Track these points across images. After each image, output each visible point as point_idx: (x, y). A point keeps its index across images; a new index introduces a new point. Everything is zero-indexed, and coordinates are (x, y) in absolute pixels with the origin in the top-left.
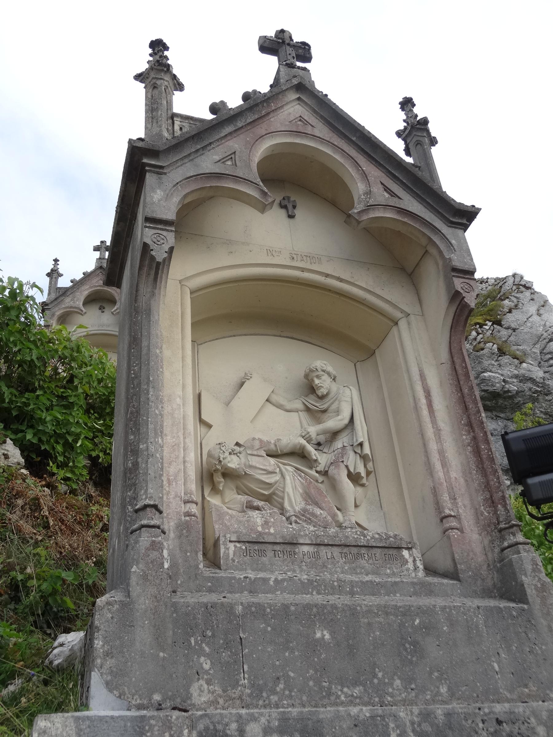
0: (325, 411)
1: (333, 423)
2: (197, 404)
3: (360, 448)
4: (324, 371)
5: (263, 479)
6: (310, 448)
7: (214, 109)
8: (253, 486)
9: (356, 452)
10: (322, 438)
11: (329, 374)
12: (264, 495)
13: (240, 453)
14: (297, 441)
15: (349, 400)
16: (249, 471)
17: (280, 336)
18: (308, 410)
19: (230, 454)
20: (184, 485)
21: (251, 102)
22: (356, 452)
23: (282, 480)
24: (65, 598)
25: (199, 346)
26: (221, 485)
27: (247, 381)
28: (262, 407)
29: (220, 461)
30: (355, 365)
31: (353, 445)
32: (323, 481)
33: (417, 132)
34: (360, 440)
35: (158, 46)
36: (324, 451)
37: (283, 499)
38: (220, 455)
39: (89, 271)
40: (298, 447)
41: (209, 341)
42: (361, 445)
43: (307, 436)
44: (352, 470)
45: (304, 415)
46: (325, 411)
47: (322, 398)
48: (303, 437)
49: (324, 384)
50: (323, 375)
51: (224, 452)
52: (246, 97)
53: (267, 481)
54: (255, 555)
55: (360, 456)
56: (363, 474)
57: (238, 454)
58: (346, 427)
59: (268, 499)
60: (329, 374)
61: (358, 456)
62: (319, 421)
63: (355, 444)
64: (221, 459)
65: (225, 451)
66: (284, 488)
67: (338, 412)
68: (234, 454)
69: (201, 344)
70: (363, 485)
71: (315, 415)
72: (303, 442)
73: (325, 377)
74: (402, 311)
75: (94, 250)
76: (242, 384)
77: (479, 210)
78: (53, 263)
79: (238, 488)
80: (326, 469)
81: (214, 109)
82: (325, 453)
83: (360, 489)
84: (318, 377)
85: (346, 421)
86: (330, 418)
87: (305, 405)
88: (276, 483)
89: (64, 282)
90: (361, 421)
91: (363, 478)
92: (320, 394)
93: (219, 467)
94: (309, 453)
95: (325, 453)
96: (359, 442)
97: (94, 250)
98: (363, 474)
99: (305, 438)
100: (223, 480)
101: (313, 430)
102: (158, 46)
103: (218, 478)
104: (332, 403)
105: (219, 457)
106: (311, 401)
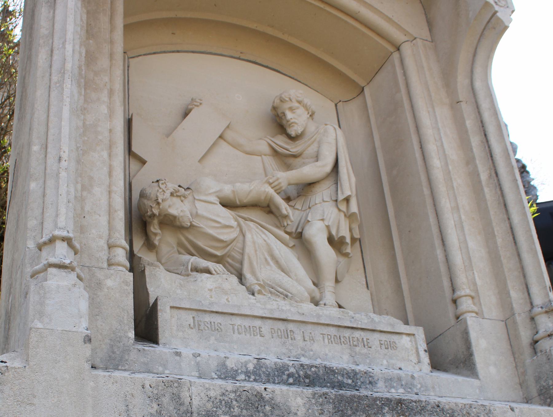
1: (308, 171)
2: (127, 133)
3: (345, 203)
4: (299, 102)
5: (215, 235)
6: (279, 200)
8: (201, 243)
10: (292, 192)
11: (306, 107)
13: (185, 197)
14: (263, 189)
15: (334, 142)
16: (196, 222)
17: (239, 59)
18: (275, 153)
19: (172, 194)
22: (340, 210)
23: (241, 238)
25: (130, 60)
26: (158, 238)
27: (196, 108)
28: (215, 144)
29: (158, 204)
30: (336, 105)
31: (336, 201)
32: (294, 246)
34: (348, 193)
36: (296, 207)
37: (241, 263)
38: (158, 194)
40: (263, 198)
41: (144, 55)
42: (347, 200)
43: (276, 183)
44: (334, 232)
45: (270, 161)
46: (295, 156)
47: (293, 139)
48: (270, 184)
49: (297, 120)
50: (298, 108)
51: (163, 191)
53: (222, 237)
54: (206, 328)
55: (345, 215)
56: (348, 240)
57: (183, 198)
58: (328, 176)
60: (306, 107)
61: (342, 215)
62: (288, 167)
64: (160, 201)
65: (165, 189)
66: (243, 249)
67: (317, 158)
68: (177, 196)
69: (133, 57)
70: (346, 255)
71: (285, 160)
72: (271, 191)
73: (301, 111)
74: (406, 33)
76: (186, 114)
79: (180, 245)
80: (299, 230)
82: (298, 209)
83: (343, 260)
84: (291, 109)
85: (328, 168)
86: (304, 164)
88: (233, 241)
90: (347, 170)
91: (347, 244)
92: (293, 134)
93: (156, 212)
94: (278, 208)
95: (298, 209)
96: (345, 196)
98: (348, 240)
99: (273, 185)
100: (159, 231)
101: (285, 177)
103: (154, 228)
104: (309, 146)
105: (157, 197)
106: (280, 141)
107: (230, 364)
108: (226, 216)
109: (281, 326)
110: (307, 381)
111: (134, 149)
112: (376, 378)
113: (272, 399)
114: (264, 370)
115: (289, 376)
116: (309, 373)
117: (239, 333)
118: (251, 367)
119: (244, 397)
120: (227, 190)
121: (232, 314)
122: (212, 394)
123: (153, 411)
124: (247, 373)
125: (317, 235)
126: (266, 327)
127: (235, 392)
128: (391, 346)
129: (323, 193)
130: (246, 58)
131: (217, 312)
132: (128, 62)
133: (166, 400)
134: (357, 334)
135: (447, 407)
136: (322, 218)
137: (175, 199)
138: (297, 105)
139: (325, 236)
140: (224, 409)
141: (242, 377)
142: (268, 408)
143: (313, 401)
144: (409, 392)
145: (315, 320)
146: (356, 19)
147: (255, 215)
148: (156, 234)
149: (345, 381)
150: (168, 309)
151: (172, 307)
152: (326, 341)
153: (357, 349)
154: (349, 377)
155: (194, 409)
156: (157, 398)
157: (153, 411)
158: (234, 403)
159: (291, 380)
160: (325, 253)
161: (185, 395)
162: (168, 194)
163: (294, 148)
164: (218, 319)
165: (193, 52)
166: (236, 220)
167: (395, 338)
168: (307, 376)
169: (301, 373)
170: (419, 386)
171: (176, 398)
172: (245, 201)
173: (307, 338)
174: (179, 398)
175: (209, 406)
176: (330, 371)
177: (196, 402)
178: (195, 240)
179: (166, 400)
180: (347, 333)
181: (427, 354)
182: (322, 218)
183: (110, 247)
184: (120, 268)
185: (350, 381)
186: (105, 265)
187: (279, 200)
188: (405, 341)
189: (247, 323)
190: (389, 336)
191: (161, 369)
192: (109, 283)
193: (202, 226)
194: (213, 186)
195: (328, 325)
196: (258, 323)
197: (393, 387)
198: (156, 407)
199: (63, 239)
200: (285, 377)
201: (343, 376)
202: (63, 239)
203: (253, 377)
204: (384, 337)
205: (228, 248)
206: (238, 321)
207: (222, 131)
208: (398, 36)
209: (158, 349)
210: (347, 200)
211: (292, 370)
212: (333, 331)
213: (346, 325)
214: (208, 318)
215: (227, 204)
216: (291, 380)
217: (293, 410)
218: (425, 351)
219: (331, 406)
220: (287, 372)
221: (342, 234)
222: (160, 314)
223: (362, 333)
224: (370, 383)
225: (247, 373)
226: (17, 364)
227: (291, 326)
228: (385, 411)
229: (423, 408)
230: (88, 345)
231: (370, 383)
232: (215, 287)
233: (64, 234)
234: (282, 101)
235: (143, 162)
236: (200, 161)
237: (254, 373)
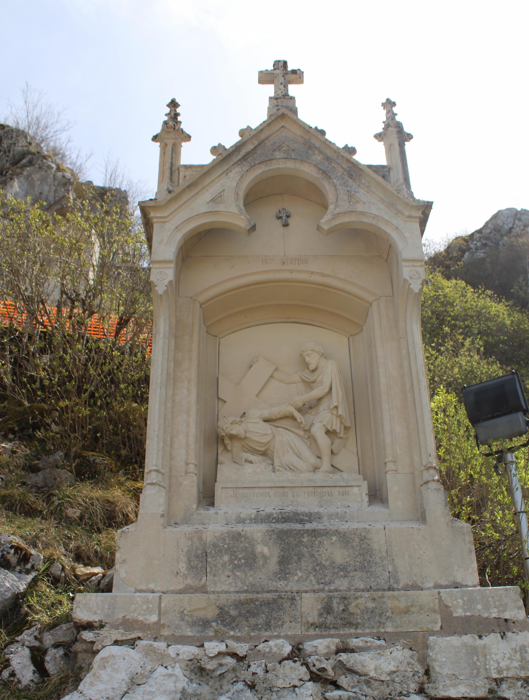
0: (314, 382)
4: (312, 350)
6: (297, 414)
7: (214, 150)
8: (252, 445)
9: (333, 414)
12: (261, 451)
16: (248, 435)
17: (287, 322)
20: (377, 589)
21: (247, 136)
24: (71, 332)
26: (229, 446)
28: (267, 382)
29: (224, 430)
30: (349, 339)
33: (395, 135)
35: (173, 104)
37: (273, 452)
39: (253, 127)
46: (314, 382)
52: (242, 133)
59: (264, 454)
63: (332, 407)
64: (224, 429)
75: (262, 81)
76: (251, 367)
77: (432, 203)
78: (168, 110)
79: (243, 446)
81: (214, 150)
84: (308, 355)
85: (327, 390)
87: (301, 377)
89: (195, 154)
97: (262, 81)
102: (173, 104)
103: (227, 441)
107: (242, 516)
108: (267, 428)
109: (281, 490)
110: (283, 520)
111: (219, 396)
112: (323, 515)
113: (245, 535)
114: (260, 517)
115: (273, 519)
116: (284, 516)
117: (258, 497)
118: (253, 516)
119: (231, 535)
120: (266, 414)
121: (254, 487)
122: (216, 535)
123: (189, 545)
124: (251, 520)
125: (318, 431)
126: (272, 492)
127: (227, 533)
128: (344, 494)
129: (324, 405)
130: (290, 321)
131: (246, 488)
132: (219, 341)
133: (195, 539)
134: (325, 490)
135: (342, 531)
136: (322, 420)
137: (234, 426)
138: (311, 352)
139: (323, 431)
140: (221, 541)
141: (248, 521)
142: (243, 539)
143: (266, 534)
144: (342, 521)
145: (300, 485)
146: (345, 292)
147: (286, 423)
148: (228, 444)
149: (305, 518)
150: (220, 489)
151: (222, 488)
152: (306, 495)
153: (324, 498)
154: (307, 516)
155: (208, 542)
156: (191, 539)
157: (189, 545)
158: (227, 538)
159: (274, 521)
160: (323, 440)
161: (204, 537)
162: (229, 424)
163: (312, 378)
164: (246, 491)
165: (258, 325)
166: (271, 429)
167: (348, 489)
168: (283, 518)
169: (280, 516)
170: (349, 517)
171: (200, 538)
172: (278, 417)
173: (295, 495)
174: (201, 538)
175: (215, 540)
176: (296, 514)
177: (208, 539)
178: (249, 444)
179: (195, 539)
180: (319, 490)
181: (368, 496)
182: (322, 420)
183: (187, 464)
184: (191, 474)
185: (307, 518)
186: (183, 474)
187: (297, 414)
188: (356, 490)
189: (262, 491)
190: (345, 488)
191: (208, 521)
192: (185, 483)
193: (251, 436)
194: (256, 414)
195: (308, 487)
196: (268, 490)
197: (333, 519)
198: (190, 542)
199: (155, 471)
200: (271, 519)
201: (303, 516)
202: (155, 471)
203: (254, 521)
204: (342, 489)
205: (267, 446)
206: (257, 491)
207: (271, 373)
208: (369, 298)
209: (212, 511)
210: (336, 407)
211: (275, 515)
212: (311, 490)
213: (318, 485)
214: (241, 491)
215: (266, 421)
216: (274, 521)
217: (256, 539)
218: (367, 494)
219: (275, 536)
220: (272, 517)
221: (334, 428)
222: (216, 492)
223: (329, 489)
224: (319, 518)
225: (251, 520)
226: (133, 529)
227: (286, 490)
228: (305, 536)
229: (327, 533)
230: (162, 518)
231: (319, 518)
232: (255, 471)
233: (155, 468)
234: (303, 351)
235: (225, 402)
236: (256, 396)
237: (255, 519)
